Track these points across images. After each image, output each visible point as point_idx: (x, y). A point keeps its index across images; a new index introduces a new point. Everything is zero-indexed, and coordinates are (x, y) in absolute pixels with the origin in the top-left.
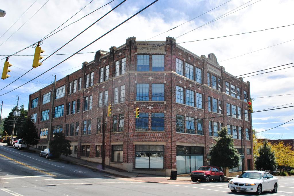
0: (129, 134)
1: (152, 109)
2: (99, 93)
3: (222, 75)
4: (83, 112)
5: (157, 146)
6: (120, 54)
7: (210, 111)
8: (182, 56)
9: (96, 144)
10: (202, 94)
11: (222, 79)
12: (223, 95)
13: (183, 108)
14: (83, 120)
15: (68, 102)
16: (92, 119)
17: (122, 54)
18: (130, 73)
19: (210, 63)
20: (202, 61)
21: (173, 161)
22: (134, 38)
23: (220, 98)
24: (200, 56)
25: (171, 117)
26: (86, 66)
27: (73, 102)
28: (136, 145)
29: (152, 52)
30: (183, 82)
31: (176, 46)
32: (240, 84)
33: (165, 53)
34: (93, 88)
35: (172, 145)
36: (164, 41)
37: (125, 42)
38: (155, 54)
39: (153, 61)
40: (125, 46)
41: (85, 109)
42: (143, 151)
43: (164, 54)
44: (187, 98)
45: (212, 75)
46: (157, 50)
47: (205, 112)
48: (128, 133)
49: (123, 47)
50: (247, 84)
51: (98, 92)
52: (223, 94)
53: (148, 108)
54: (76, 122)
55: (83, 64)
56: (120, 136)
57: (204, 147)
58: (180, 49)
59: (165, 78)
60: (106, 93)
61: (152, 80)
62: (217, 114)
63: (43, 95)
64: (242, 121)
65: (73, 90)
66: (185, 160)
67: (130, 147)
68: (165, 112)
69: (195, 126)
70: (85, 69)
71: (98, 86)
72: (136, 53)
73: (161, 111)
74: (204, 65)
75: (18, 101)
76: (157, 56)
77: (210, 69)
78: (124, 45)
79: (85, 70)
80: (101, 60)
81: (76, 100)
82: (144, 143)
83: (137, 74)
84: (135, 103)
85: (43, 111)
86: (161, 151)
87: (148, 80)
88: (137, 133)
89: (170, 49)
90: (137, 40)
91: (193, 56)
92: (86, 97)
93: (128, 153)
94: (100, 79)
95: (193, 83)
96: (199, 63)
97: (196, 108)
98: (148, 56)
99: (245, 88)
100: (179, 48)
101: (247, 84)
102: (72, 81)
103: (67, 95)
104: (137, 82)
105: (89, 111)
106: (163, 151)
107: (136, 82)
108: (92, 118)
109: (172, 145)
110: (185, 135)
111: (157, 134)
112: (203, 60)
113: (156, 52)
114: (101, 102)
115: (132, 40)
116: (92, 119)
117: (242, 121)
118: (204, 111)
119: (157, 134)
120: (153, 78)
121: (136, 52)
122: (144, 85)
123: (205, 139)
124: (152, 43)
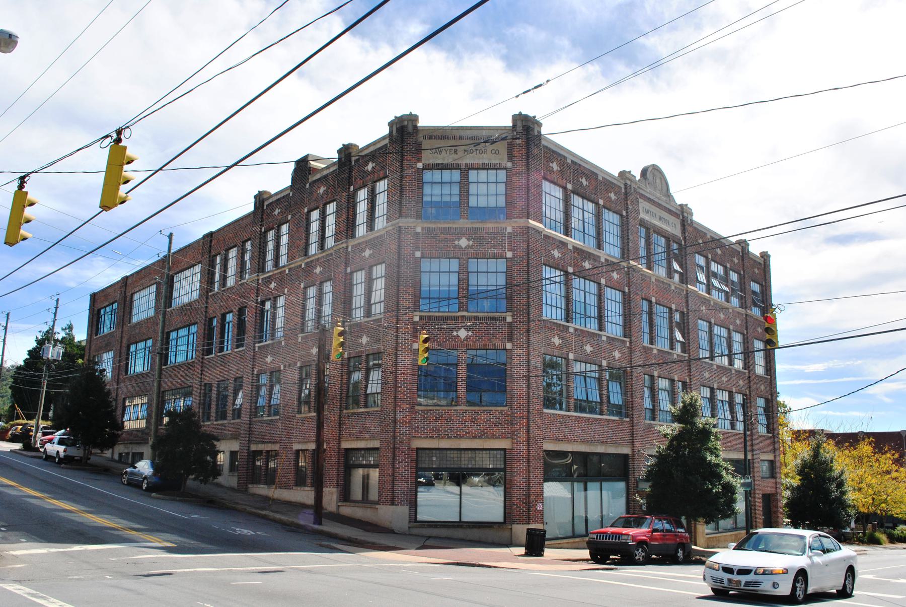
0: (399, 416)
1: (467, 338)
2: (305, 288)
3: (684, 231)
4: (254, 347)
5: (484, 452)
6: (370, 167)
7: (646, 343)
9: (296, 447)
10: (624, 292)
13: (563, 334)
14: (255, 373)
16: (282, 368)
17: (377, 167)
18: (400, 227)
20: (623, 191)
21: (532, 498)
22: (413, 118)
23: (677, 305)
26: (266, 203)
27: (224, 316)
28: (418, 449)
29: (468, 160)
31: (543, 142)
33: (509, 165)
34: (287, 272)
35: (529, 450)
36: (505, 128)
37: (386, 131)
39: (473, 189)
40: (387, 141)
42: (441, 466)
43: (505, 169)
44: (578, 303)
46: (485, 155)
48: (395, 412)
49: (379, 146)
51: (302, 285)
52: (687, 291)
54: (236, 379)
55: (256, 197)
56: (368, 422)
57: (628, 454)
59: (509, 243)
60: (328, 287)
61: (468, 247)
63: (132, 294)
64: (745, 373)
65: (224, 278)
67: (400, 457)
68: (509, 346)
72: (420, 165)
74: (629, 202)
75: (55, 314)
81: (236, 310)
82: (444, 444)
84: (416, 319)
86: (495, 467)
87: (455, 247)
88: (423, 411)
89: (524, 152)
90: (421, 123)
93: (393, 475)
94: (307, 245)
95: (596, 258)
96: (612, 196)
99: (754, 272)
103: (207, 295)
104: (422, 253)
105: (273, 344)
106: (503, 466)
107: (418, 254)
108: (285, 366)
109: (529, 450)
111: (484, 417)
112: (625, 184)
113: (481, 162)
114: (310, 314)
115: (406, 123)
116: (282, 368)
118: (628, 344)
119: (484, 417)
120: (471, 243)
121: (419, 160)
122: (445, 264)
123: (752, 443)
124: (469, 133)
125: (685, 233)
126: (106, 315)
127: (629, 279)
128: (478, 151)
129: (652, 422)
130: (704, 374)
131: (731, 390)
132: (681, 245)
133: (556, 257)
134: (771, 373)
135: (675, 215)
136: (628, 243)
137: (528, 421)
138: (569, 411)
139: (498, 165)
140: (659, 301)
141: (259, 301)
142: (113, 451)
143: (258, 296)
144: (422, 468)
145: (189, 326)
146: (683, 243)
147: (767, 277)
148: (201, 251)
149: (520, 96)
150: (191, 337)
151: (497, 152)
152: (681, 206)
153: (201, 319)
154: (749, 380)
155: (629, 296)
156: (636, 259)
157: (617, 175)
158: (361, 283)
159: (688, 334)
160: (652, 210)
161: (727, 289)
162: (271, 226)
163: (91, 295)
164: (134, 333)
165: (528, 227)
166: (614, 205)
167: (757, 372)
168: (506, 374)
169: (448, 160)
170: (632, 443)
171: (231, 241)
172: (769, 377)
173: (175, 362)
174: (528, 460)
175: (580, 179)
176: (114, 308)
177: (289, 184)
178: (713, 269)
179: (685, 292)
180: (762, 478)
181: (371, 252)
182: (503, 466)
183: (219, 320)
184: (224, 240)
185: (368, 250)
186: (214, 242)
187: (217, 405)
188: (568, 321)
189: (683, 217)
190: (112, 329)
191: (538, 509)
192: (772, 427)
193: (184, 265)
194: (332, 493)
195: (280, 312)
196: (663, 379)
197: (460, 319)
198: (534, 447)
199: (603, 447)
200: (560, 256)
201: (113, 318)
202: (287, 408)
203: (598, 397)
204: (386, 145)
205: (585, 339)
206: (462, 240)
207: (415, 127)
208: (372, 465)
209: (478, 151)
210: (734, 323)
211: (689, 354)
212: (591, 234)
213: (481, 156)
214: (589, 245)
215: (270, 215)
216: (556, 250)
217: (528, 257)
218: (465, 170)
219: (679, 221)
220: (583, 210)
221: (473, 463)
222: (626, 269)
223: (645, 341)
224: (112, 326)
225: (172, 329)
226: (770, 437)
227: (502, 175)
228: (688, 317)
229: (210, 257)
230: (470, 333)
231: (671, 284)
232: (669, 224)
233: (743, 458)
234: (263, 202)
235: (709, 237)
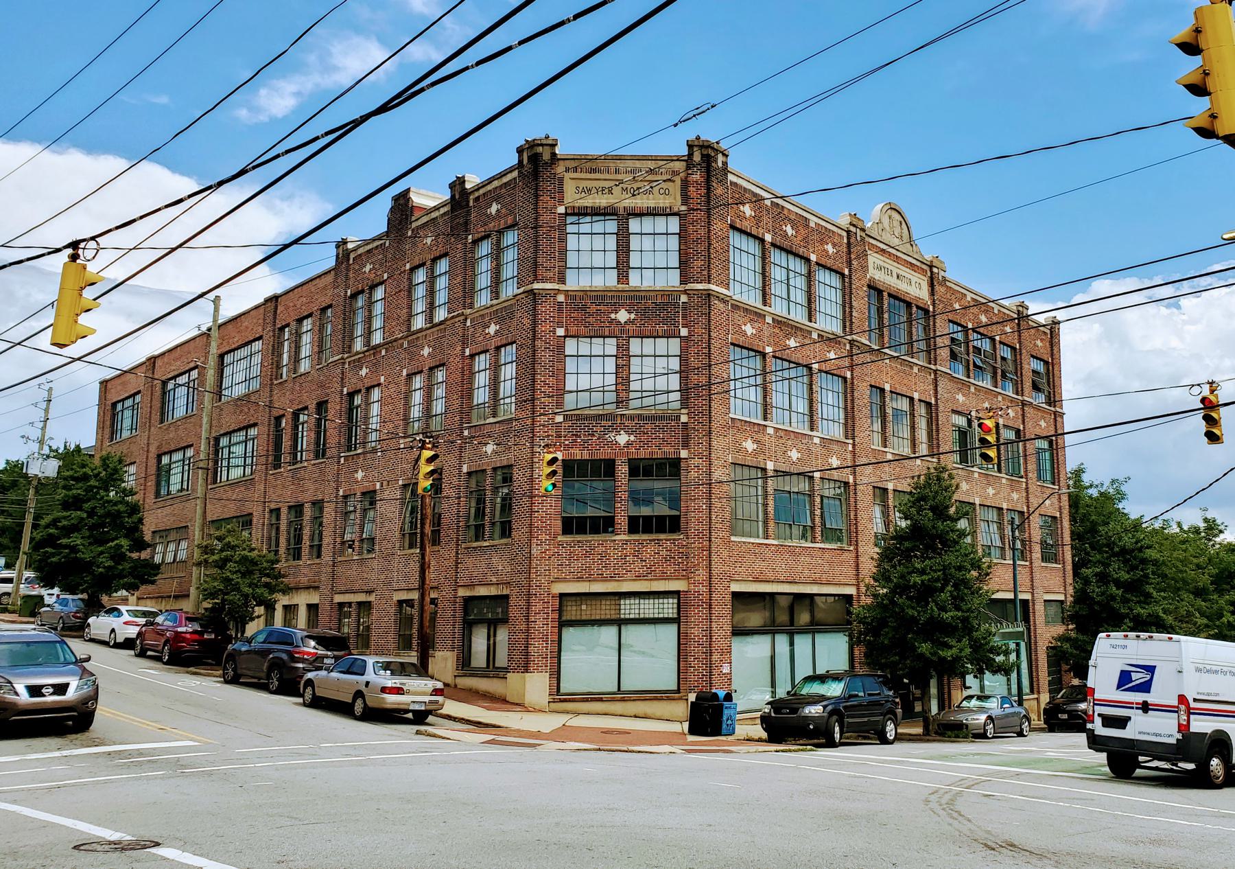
1: (628, 444)
6: (494, 208)
7: (877, 446)
8: (757, 219)
11: (934, 311)
13: (759, 436)
14: (341, 493)
15: (276, 413)
16: (378, 487)
17: (504, 211)
20: (845, 241)
21: (715, 657)
26: (352, 256)
27: (296, 415)
37: (514, 160)
38: (640, 214)
39: (634, 243)
40: (515, 174)
41: (112, 440)
51: (405, 373)
54: (314, 503)
59: (684, 317)
61: (629, 322)
65: (296, 360)
67: (537, 606)
70: (348, 270)
71: (405, 345)
75: (47, 410)
76: (648, 224)
77: (878, 269)
78: (511, 170)
79: (347, 275)
80: (413, 230)
81: (312, 407)
85: (165, 453)
89: (703, 191)
92: (351, 390)
94: (410, 316)
95: (806, 333)
96: (830, 248)
97: (819, 434)
98: (612, 226)
99: (1035, 345)
102: (294, 325)
104: (567, 330)
106: (675, 616)
114: (416, 412)
115: (540, 149)
116: (378, 487)
118: (850, 447)
120: (633, 316)
122: (597, 346)
126: (125, 412)
131: (1000, 506)
132: (929, 311)
133: (749, 334)
134: (1059, 482)
140: (896, 388)
141: (345, 393)
142: (760, 740)
143: (343, 387)
145: (246, 428)
146: (931, 309)
148: (261, 321)
149: (679, 125)
150: (250, 444)
151: (666, 193)
153: (263, 417)
158: (485, 370)
162: (360, 289)
163: (101, 383)
164: (166, 438)
171: (303, 307)
173: (228, 480)
174: (710, 605)
175: (784, 227)
176: (136, 401)
177: (386, 230)
181: (498, 327)
182: (675, 616)
183: (290, 420)
184: (295, 306)
185: (493, 325)
186: (280, 309)
187: (288, 541)
190: (134, 431)
191: (724, 672)
192: (1061, 555)
193: (237, 341)
194: (446, 659)
195: (375, 409)
197: (619, 418)
198: (718, 587)
200: (754, 332)
201: (135, 416)
202: (385, 542)
203: (809, 519)
204: (515, 179)
205: (790, 442)
206: (620, 312)
207: (554, 154)
208: (500, 619)
212: (799, 301)
214: (798, 315)
215: (358, 272)
216: (749, 324)
217: (709, 336)
218: (623, 217)
220: (788, 269)
222: (1016, 321)
223: (876, 442)
224: (134, 427)
225: (222, 432)
227: (674, 224)
228: (937, 409)
229: (274, 331)
230: (632, 438)
232: (910, 284)
233: (1013, 597)
234: (348, 255)
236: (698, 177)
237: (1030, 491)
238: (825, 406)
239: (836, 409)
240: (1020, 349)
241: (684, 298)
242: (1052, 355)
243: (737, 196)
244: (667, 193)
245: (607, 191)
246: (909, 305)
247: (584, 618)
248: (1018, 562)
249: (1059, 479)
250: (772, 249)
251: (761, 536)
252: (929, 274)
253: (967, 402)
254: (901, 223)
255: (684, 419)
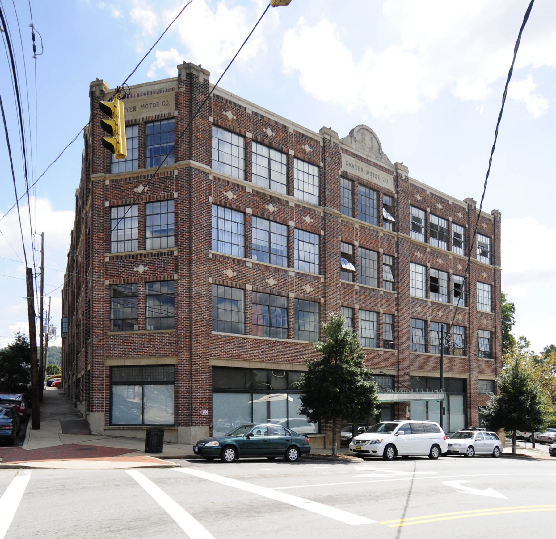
1: (145, 272)
3: (397, 185)
5: (160, 368)
10: (320, 235)
12: (398, 240)
19: (351, 151)
23: (385, 249)
24: (489, 213)
25: (190, 289)
30: (455, 266)
31: (410, 181)
32: (463, 214)
35: (191, 365)
36: (172, 80)
45: (359, 184)
46: (157, 108)
47: (324, 284)
50: (492, 218)
52: (495, 270)
53: (135, 269)
58: (227, 101)
62: (374, 290)
64: (465, 310)
66: (140, 402)
69: (393, 333)
73: (167, 275)
74: (327, 155)
82: (129, 362)
83: (110, 181)
84: (107, 259)
86: (168, 380)
88: (114, 336)
91: (285, 127)
97: (430, 300)
100: (223, 99)
101: (492, 218)
104: (110, 203)
109: (191, 365)
110: (245, 339)
112: (324, 139)
117: (467, 311)
118: (322, 280)
123: (470, 366)
124: (144, 90)
125: (398, 187)
127: (325, 223)
128: (152, 105)
129: (378, 349)
130: (416, 309)
134: (495, 310)
135: (389, 172)
136: (325, 191)
137: (190, 341)
138: (246, 334)
139: (168, 115)
144: (114, 382)
147: (497, 231)
152: (396, 164)
154: (469, 315)
155: (325, 238)
156: (339, 206)
157: (318, 132)
159: (398, 274)
160: (358, 165)
161: (394, 220)
165: (191, 168)
166: (230, 124)
167: (411, 294)
168: (174, 301)
169: (128, 117)
170: (470, 372)
172: (493, 313)
178: (479, 240)
179: (396, 239)
180: (479, 394)
188: (353, 281)
189: (397, 173)
191: (203, 414)
196: (482, 331)
197: (139, 257)
199: (289, 366)
205: (267, 274)
207: (102, 91)
209: (152, 105)
210: (455, 268)
211: (398, 291)
213: (154, 109)
219: (392, 177)
221: (152, 377)
226: (465, 359)
228: (398, 260)
231: (379, 231)
233: (440, 376)
235: (428, 193)
236: (184, 89)
237: (471, 314)
238: (487, 297)
239: (487, 299)
240: (469, 228)
241: (176, 173)
242: (494, 233)
243: (220, 104)
244: (167, 104)
245: (132, 109)
246: (378, 192)
247: (124, 380)
248: (444, 355)
249: (495, 308)
250: (453, 224)
251: (243, 333)
252: (395, 174)
253: (424, 258)
254: (371, 138)
255: (176, 254)
